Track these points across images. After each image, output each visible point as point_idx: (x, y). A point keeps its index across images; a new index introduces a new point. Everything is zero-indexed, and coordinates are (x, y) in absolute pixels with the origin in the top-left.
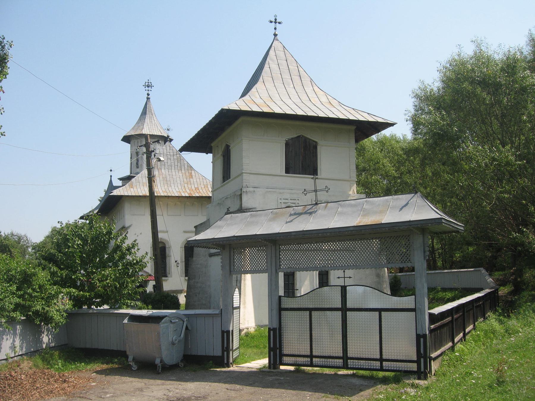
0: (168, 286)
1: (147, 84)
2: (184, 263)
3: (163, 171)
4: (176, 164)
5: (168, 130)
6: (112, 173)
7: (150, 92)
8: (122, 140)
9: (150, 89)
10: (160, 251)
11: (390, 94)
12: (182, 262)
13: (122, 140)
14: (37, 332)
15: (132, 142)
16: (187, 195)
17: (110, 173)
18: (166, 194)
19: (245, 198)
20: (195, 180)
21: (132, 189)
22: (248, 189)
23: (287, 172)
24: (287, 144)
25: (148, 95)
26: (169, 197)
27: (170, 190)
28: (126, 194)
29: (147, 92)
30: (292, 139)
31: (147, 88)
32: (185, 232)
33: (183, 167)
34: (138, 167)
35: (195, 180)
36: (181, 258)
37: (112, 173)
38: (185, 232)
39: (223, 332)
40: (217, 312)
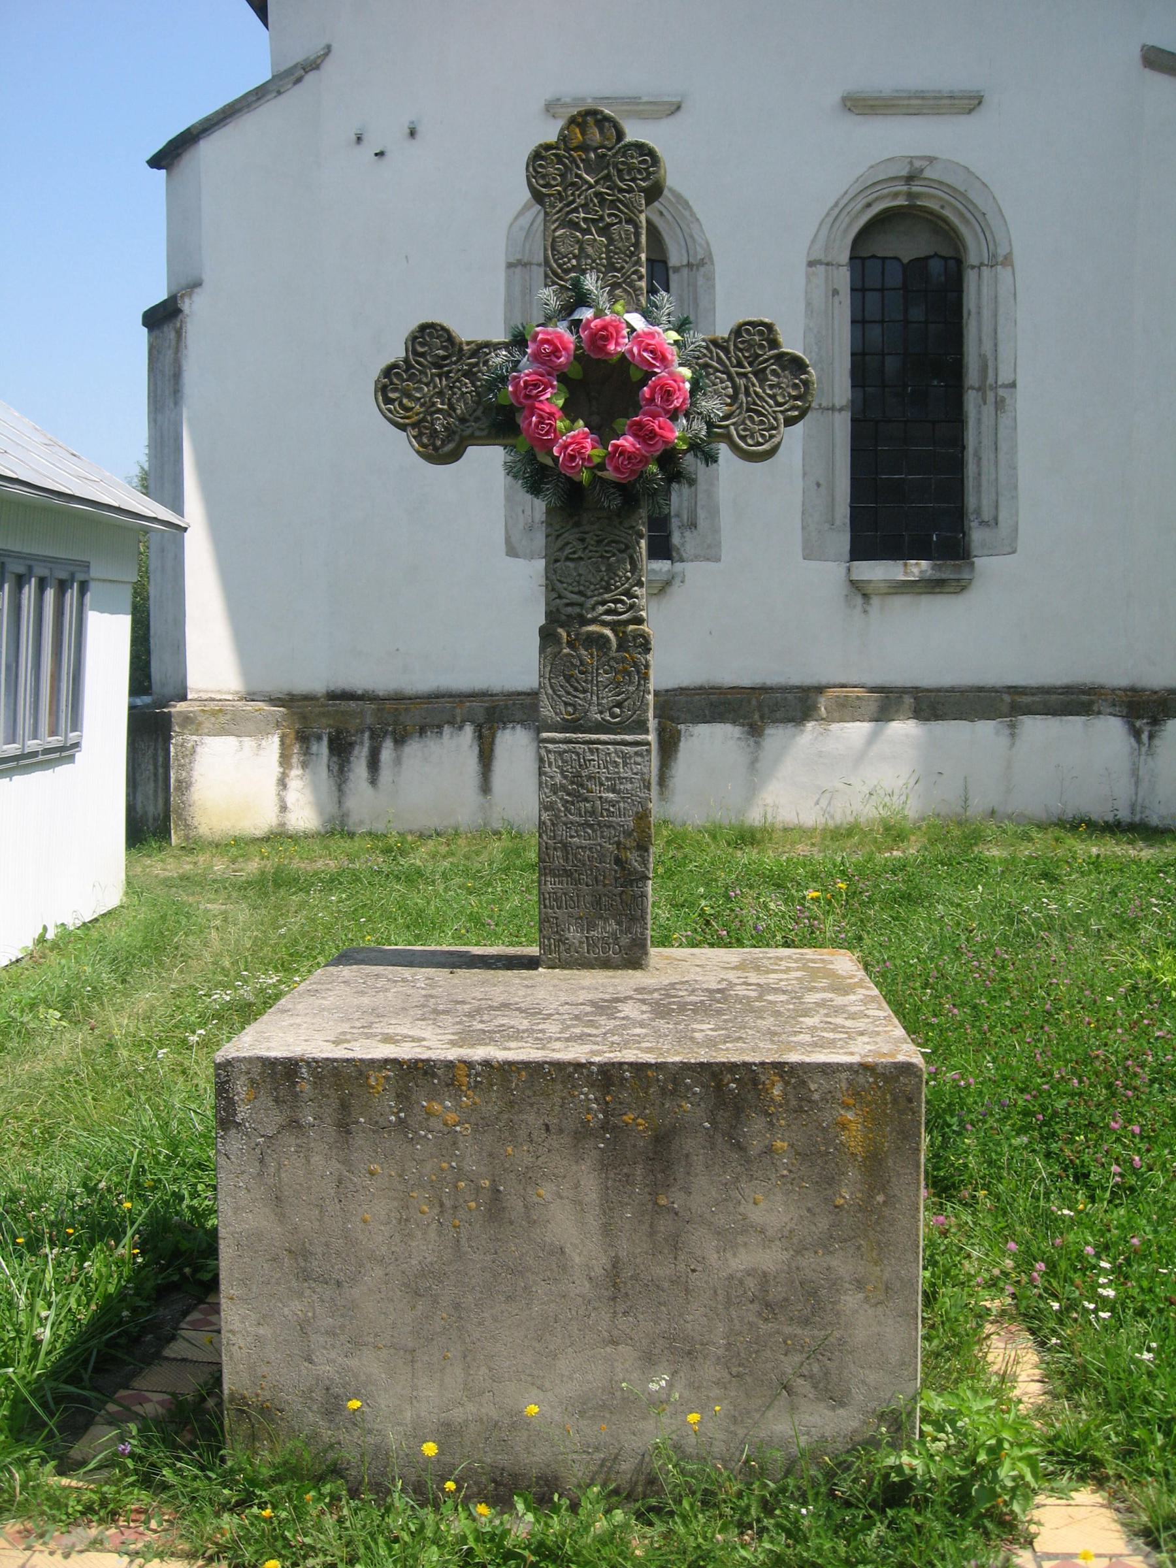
32: (860, 105)
38: (860, 105)
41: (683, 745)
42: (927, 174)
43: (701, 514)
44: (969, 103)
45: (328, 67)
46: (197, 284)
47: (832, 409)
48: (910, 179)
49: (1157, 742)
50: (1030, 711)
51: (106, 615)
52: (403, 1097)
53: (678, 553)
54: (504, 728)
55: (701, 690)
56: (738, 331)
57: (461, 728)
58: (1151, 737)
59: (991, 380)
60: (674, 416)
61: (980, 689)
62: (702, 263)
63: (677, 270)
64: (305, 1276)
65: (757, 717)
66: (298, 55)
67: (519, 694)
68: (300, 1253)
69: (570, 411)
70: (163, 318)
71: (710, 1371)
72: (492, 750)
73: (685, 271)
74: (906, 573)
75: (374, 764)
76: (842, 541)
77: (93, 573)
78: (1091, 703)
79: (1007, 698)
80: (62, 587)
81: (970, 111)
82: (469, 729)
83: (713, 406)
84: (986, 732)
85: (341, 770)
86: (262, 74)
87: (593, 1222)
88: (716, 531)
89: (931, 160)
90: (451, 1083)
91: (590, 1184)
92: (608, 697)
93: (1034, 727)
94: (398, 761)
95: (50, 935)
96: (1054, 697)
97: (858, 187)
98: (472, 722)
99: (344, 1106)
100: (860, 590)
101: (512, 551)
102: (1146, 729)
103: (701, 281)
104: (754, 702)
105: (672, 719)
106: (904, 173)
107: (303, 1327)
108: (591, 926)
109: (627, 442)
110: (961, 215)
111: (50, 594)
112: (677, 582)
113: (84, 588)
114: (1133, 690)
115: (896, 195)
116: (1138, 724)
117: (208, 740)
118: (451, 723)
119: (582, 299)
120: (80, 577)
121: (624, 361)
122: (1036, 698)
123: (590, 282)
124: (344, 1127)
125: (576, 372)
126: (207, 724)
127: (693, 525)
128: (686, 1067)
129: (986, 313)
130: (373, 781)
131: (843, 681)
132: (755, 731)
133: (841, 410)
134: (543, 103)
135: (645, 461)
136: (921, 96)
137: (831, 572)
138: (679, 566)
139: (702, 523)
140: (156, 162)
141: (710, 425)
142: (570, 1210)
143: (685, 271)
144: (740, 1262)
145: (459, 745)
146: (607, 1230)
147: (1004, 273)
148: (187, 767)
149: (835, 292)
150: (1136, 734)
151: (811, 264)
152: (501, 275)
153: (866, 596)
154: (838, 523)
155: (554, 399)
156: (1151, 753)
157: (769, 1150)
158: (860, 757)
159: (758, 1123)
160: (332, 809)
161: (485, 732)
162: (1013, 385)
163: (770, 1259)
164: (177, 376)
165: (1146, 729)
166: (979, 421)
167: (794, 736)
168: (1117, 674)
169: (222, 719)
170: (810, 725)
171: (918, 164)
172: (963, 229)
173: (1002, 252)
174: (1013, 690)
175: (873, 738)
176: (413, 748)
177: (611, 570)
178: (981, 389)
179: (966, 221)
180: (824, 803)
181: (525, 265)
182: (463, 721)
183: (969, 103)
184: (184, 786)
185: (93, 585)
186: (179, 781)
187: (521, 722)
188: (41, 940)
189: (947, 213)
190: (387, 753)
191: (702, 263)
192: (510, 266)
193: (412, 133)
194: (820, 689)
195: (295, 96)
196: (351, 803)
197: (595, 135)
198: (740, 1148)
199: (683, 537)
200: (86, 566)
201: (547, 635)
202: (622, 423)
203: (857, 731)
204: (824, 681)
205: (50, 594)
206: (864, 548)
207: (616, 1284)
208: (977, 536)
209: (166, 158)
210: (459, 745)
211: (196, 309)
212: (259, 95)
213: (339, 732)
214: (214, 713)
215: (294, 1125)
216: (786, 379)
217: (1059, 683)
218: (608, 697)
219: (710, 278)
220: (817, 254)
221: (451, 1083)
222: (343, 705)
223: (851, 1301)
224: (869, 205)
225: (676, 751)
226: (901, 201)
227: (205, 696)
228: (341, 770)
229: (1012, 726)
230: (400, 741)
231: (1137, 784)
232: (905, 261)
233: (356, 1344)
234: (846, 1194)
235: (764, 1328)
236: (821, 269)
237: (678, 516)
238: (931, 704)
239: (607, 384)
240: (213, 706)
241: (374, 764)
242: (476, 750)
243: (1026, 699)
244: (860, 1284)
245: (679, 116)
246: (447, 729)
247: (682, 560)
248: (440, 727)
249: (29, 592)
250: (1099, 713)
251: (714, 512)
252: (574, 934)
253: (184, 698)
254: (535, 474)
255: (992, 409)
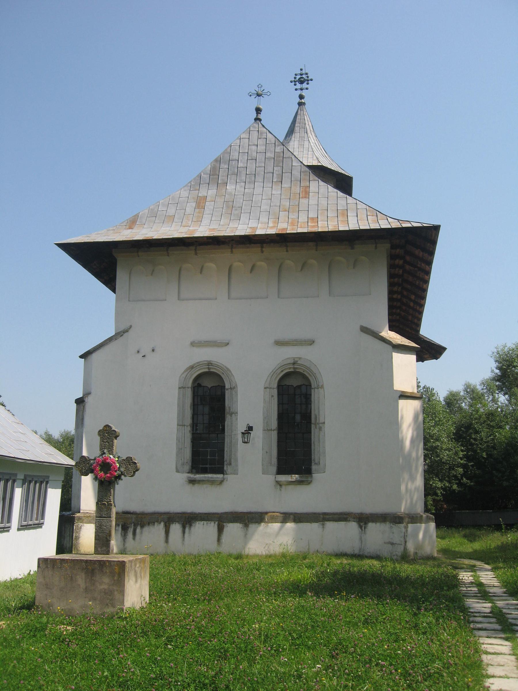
1: (298, 77)
2: (274, 435)
3: (230, 187)
4: (270, 169)
5: (259, 95)
7: (304, 93)
9: (305, 85)
12: (267, 430)
14: (465, 428)
17: (254, 102)
25: (301, 97)
29: (299, 92)
31: (299, 86)
32: (279, 343)
33: (286, 176)
36: (266, 419)
38: (279, 343)
41: (225, 529)
42: (299, 362)
43: (232, 460)
44: (311, 342)
45: (131, 332)
46: (89, 393)
47: (271, 430)
48: (294, 364)
49: (366, 530)
50: (329, 520)
51: (189, 511)
52: (61, 564)
53: (226, 472)
54: (173, 523)
55: (232, 513)
56: (127, 458)
57: (160, 523)
58: (365, 528)
59: (318, 422)
60: (116, 471)
61: (315, 514)
62: (234, 388)
63: (227, 389)
64: (47, 588)
65: (247, 521)
66: (122, 329)
67: (178, 513)
68: (47, 585)
69: (101, 470)
70: (80, 402)
71: (98, 602)
72: (169, 530)
73: (230, 390)
74: (291, 479)
75: (134, 534)
76: (274, 469)
77: (50, 479)
78: (347, 518)
79: (321, 516)
80: (41, 483)
81: (311, 345)
82: (162, 524)
83: (122, 469)
84: (315, 526)
85: (125, 535)
86: (112, 333)
87: (84, 581)
88: (237, 466)
89: (300, 358)
90: (67, 562)
91: (84, 576)
92: (106, 513)
93: (330, 525)
94: (141, 533)
95: (32, 573)
96: (335, 516)
97: (279, 366)
98: (164, 521)
99: (54, 565)
100: (279, 484)
101: (178, 471)
102: (364, 526)
103: (234, 393)
104: (246, 517)
105: (221, 521)
106: (292, 362)
107: (46, 595)
108: (102, 548)
109: (108, 475)
110: (309, 374)
111: (38, 485)
112: (225, 481)
113: (47, 483)
114: (361, 514)
115: (290, 368)
116: (361, 524)
117: (85, 524)
118: (157, 521)
119: (104, 453)
120: (46, 480)
121: (109, 463)
122: (331, 516)
123: (106, 451)
124: (53, 567)
125: (102, 464)
126: (85, 520)
127: (230, 464)
128: (96, 560)
129: (316, 402)
130: (134, 539)
131: (274, 511)
132: (246, 526)
133: (274, 430)
134: (190, 342)
135: (111, 478)
136: (296, 340)
137: (271, 478)
138: (226, 476)
139: (233, 464)
140: (81, 357)
141: (122, 472)
142: (81, 580)
143: (230, 390)
144: (102, 587)
145: (160, 528)
146: (85, 582)
147: (321, 391)
148: (79, 532)
149: (272, 396)
150: (361, 527)
151: (265, 388)
152: (177, 391)
153: (281, 485)
154: (273, 463)
155: (98, 468)
156: (365, 533)
157: (106, 572)
158: (278, 534)
159: (105, 568)
160: (121, 547)
161: (167, 524)
162: (324, 423)
163: (106, 587)
164: (83, 419)
165: (364, 526)
166: (314, 433)
167: (257, 527)
168: (356, 509)
169: (90, 519)
170: (262, 524)
171: (296, 359)
172: (310, 378)
173: (320, 384)
174: (325, 514)
175: (281, 528)
176: (146, 529)
177: (107, 494)
178: (315, 424)
179: (310, 375)
180: (266, 548)
181: (184, 388)
182: (161, 521)
183: (311, 342)
184: (78, 538)
185: (50, 482)
186: (76, 536)
187: (178, 522)
188: (29, 574)
189: (305, 373)
190: (138, 530)
191: (234, 388)
192: (179, 388)
193: (153, 350)
194: (266, 513)
195: (121, 340)
196: (127, 545)
197: (108, 429)
198: (103, 571)
199: (227, 467)
200: (48, 477)
201: (97, 503)
202: (109, 472)
203: (276, 526)
204: (268, 511)
205: (38, 485)
206: (280, 471)
207: (86, 590)
208: (314, 467)
209: (84, 356)
210: (160, 528)
211: (89, 400)
212: (110, 340)
213: (125, 524)
214: (87, 517)
215: (47, 567)
216: (133, 465)
217: (339, 512)
218: (106, 513)
219: (236, 392)
220: (267, 386)
221: (67, 562)
222: (127, 516)
223: (116, 593)
224: (282, 371)
225: (223, 531)
226: (292, 370)
227: (86, 512)
228: (125, 535)
229: (323, 525)
230: (142, 527)
231: (362, 542)
232: (295, 386)
233: (53, 597)
234: (116, 578)
235: (105, 596)
236: (268, 390)
237: (226, 461)
238: (298, 518)
239: (106, 466)
240: (88, 515)
241: (134, 534)
242: (164, 530)
243: (327, 517)
244: (117, 591)
245: (228, 346)
246: (156, 523)
247: (227, 474)
248: (154, 523)
249: (32, 485)
250: (349, 521)
251: (236, 460)
252: (99, 549)
253: (79, 512)
254: (96, 478)
255: (318, 430)
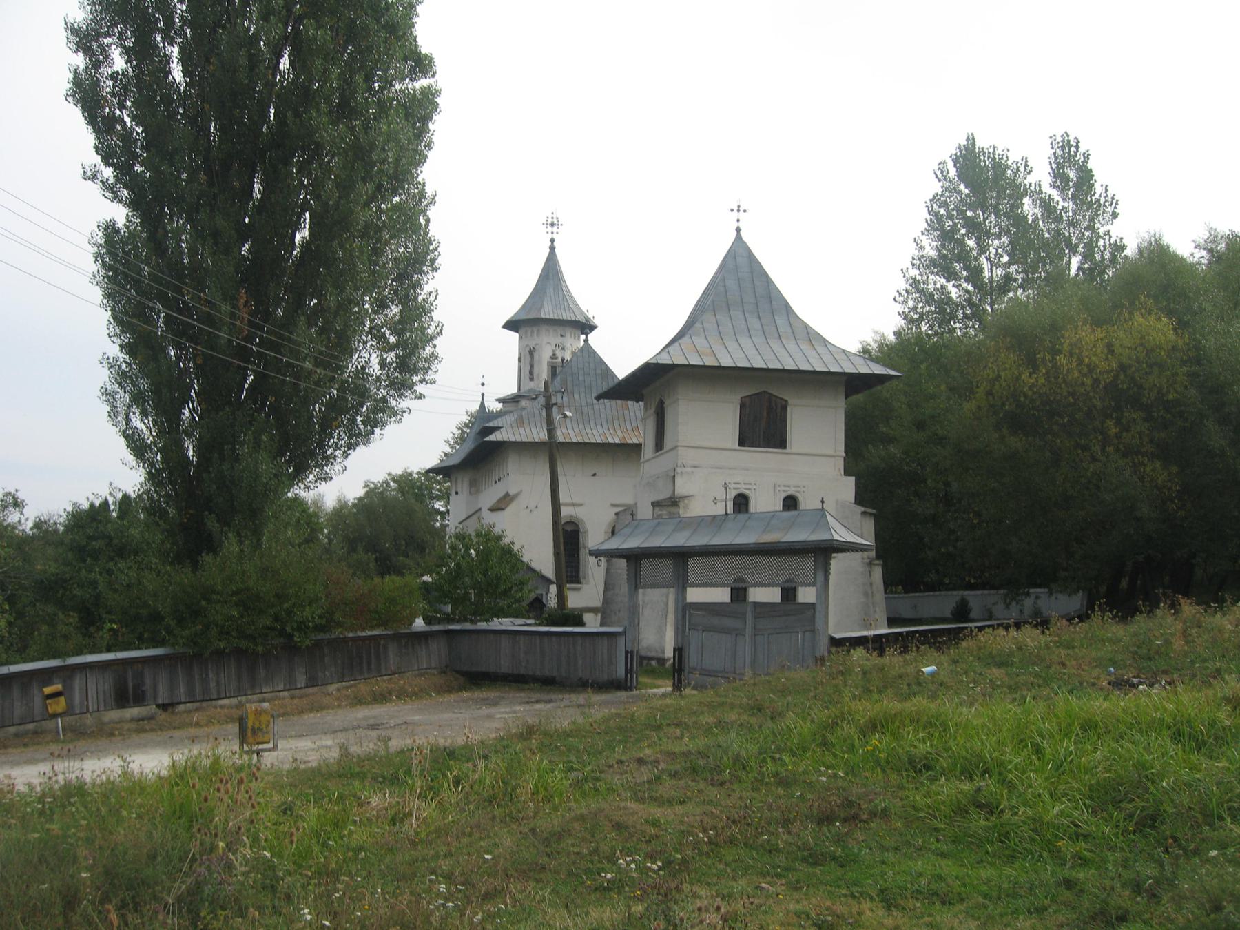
0: (574, 600)
1: (550, 220)
6: (485, 389)
7: (555, 236)
8: (504, 327)
10: (568, 539)
11: (1090, 166)
13: (504, 327)
15: (522, 330)
16: (617, 441)
18: (580, 440)
19: (678, 481)
20: (632, 414)
21: (522, 431)
22: (684, 470)
23: (741, 444)
24: (742, 406)
25: (552, 241)
26: (585, 444)
27: (589, 430)
28: (512, 439)
29: (550, 236)
30: (750, 396)
31: (550, 229)
34: (532, 379)
35: (632, 414)
37: (485, 389)
38: (614, 505)
39: (627, 652)
40: (620, 629)
